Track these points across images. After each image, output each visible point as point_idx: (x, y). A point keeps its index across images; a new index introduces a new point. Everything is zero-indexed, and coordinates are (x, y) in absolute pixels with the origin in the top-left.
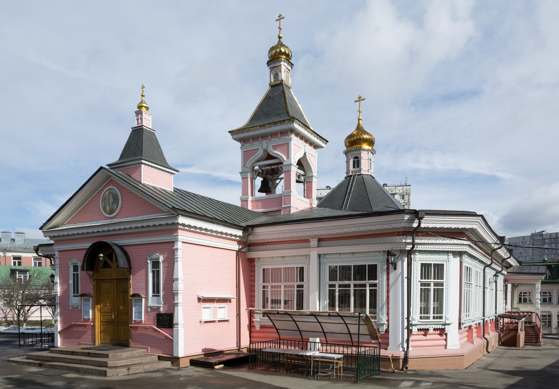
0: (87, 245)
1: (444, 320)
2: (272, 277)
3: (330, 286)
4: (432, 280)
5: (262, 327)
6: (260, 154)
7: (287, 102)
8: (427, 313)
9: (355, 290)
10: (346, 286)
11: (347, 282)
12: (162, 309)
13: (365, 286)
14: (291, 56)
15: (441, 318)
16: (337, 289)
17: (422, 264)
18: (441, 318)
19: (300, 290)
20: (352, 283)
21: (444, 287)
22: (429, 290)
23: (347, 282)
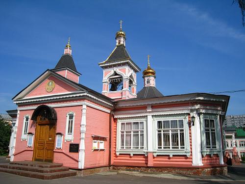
0: (35, 107)
1: (185, 149)
6: (112, 72)
7: (212, 93)
10: (176, 131)
12: (72, 141)
15: (184, 148)
18: (184, 148)
21: (184, 132)
22: (209, 133)
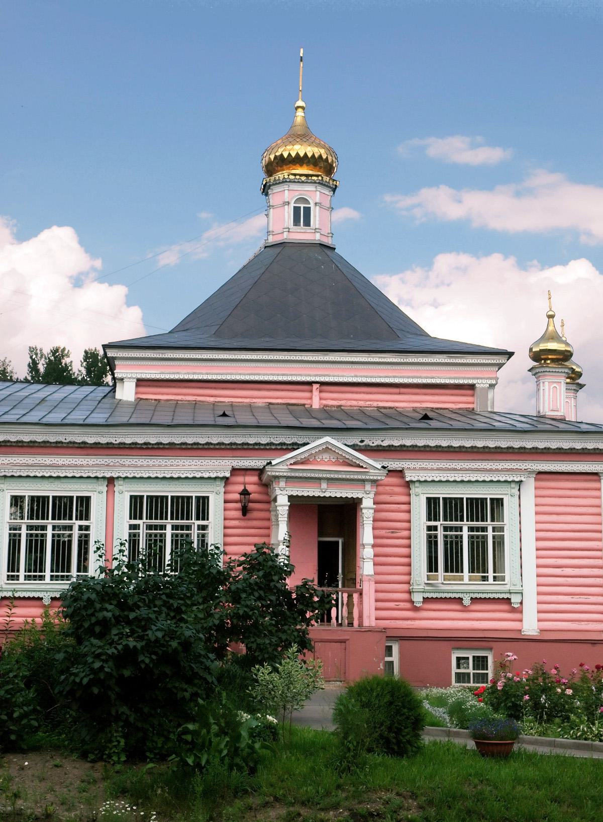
2: (462, 511)
3: (429, 528)
4: (26, 521)
5: (426, 600)
8: (41, 571)
9: (494, 537)
11: (40, 522)
13: (163, 527)
14: (330, 150)
16: (440, 533)
17: (131, 497)
19: (15, 535)
20: (50, 523)
23: (159, 522)
